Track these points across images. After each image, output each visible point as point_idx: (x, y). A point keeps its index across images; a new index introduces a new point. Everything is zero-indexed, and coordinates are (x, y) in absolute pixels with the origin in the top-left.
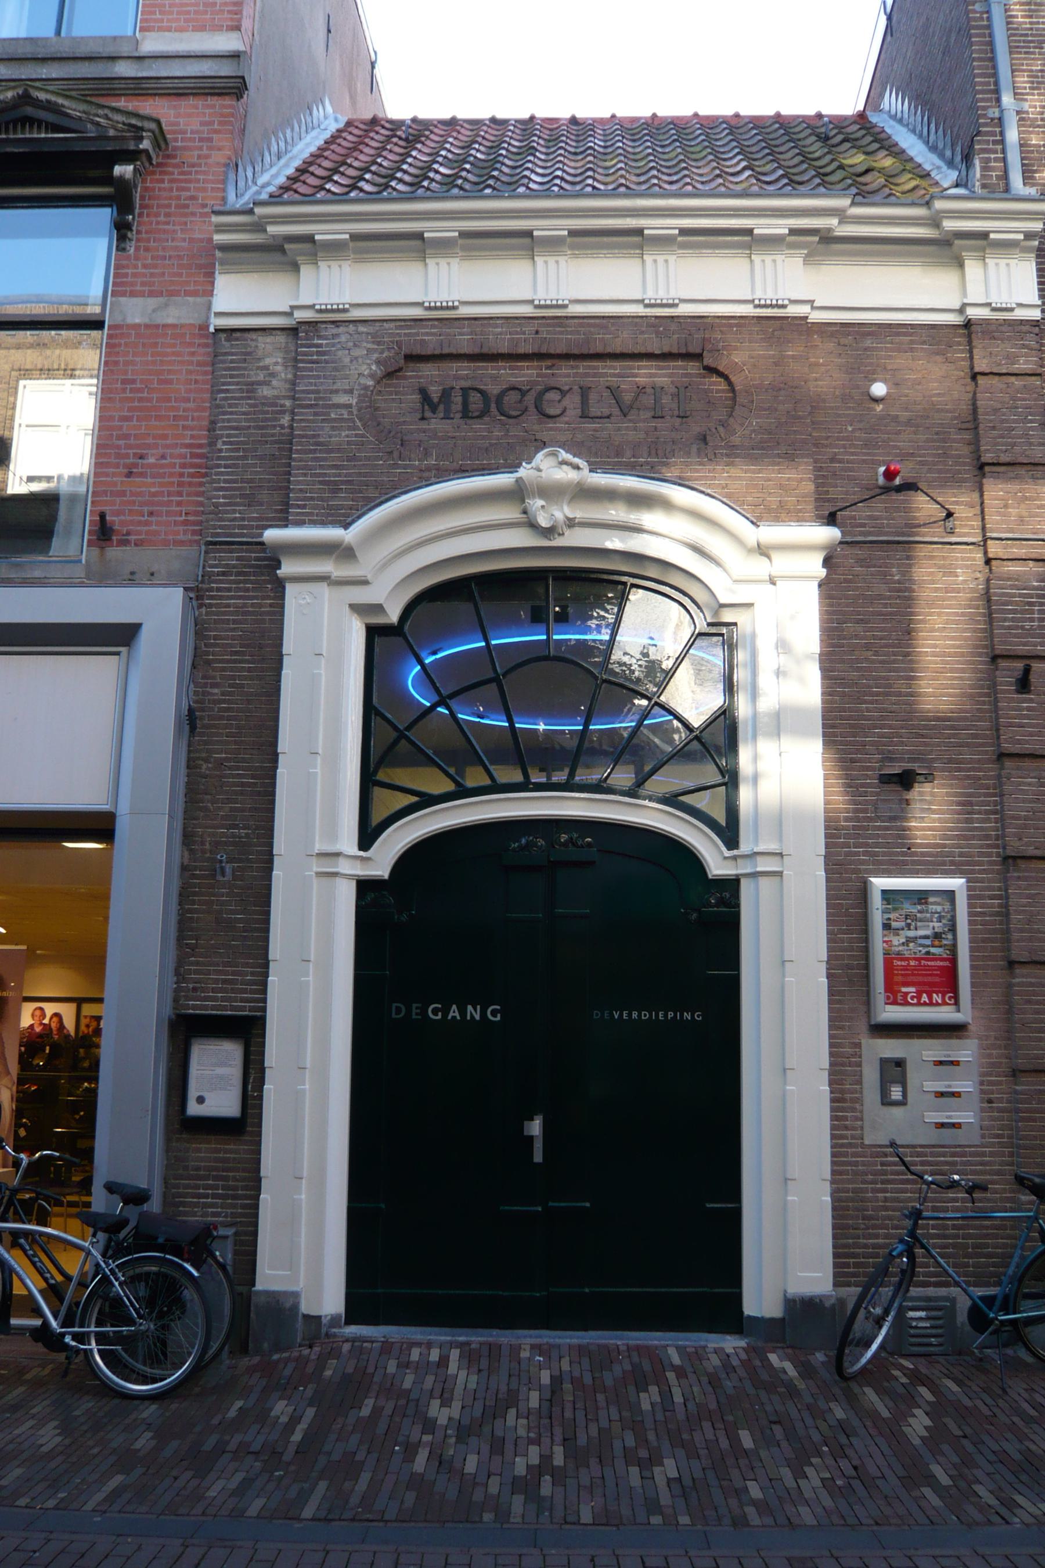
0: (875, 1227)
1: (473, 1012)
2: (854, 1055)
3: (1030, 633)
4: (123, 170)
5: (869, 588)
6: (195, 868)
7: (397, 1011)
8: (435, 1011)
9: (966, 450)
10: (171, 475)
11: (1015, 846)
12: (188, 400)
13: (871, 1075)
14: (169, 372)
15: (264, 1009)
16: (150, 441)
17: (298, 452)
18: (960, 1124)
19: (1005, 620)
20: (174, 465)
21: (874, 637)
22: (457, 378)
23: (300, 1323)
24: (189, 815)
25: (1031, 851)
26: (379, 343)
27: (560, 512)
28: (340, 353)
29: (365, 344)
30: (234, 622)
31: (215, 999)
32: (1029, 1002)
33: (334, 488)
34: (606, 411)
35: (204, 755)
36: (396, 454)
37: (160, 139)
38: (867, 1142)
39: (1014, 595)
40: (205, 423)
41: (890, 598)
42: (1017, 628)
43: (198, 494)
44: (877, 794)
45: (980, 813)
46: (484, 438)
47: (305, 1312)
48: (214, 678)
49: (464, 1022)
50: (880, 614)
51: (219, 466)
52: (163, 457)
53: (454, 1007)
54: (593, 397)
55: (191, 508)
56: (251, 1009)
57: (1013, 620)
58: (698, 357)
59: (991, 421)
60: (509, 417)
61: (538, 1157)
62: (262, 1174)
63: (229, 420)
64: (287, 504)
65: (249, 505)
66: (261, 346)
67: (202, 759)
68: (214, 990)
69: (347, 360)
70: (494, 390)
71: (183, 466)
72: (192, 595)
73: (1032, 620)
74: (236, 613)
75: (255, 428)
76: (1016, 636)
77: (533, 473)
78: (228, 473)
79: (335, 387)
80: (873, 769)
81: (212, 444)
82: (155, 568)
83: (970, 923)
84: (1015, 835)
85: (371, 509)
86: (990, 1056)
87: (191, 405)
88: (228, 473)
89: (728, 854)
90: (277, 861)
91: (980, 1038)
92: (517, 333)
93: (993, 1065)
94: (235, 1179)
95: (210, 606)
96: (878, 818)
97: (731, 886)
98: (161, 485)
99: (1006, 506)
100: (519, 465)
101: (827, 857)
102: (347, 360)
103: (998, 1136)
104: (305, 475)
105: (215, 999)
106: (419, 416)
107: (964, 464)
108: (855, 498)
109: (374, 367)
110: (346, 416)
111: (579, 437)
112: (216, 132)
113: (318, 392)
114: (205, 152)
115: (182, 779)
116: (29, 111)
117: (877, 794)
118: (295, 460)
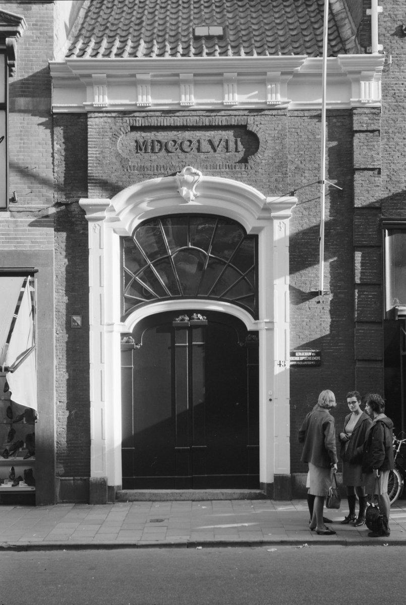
97: (256, 333)
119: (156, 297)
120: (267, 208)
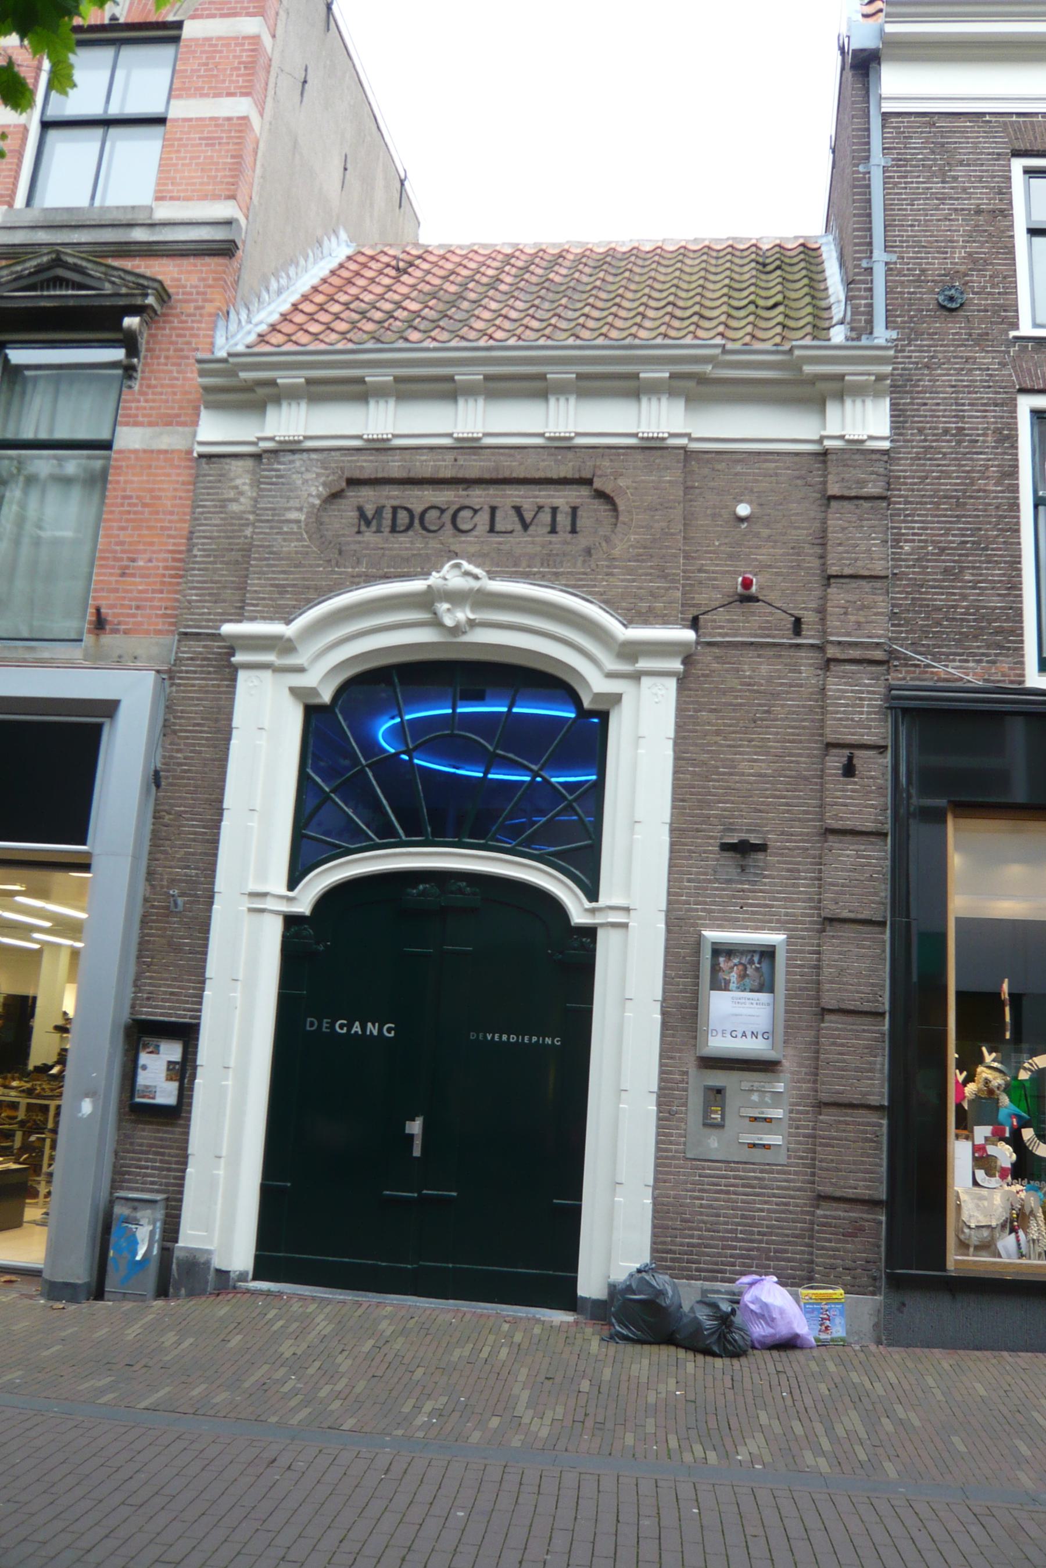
0: (691, 1229)
1: (372, 1029)
2: (682, 1082)
3: (860, 724)
4: (131, 322)
5: (723, 682)
6: (155, 900)
7: (311, 1024)
8: (341, 1027)
9: (816, 563)
10: (156, 575)
11: (831, 909)
12: (172, 513)
13: (695, 1100)
14: (160, 489)
15: (199, 1018)
16: (141, 547)
17: (255, 559)
18: (769, 1145)
19: (837, 712)
20: (158, 568)
21: (725, 725)
22: (388, 498)
23: (211, 1276)
24: (152, 858)
25: (845, 914)
26: (326, 469)
27: (462, 615)
28: (294, 476)
29: (314, 469)
30: (198, 699)
31: (164, 1007)
32: (834, 1044)
33: (282, 590)
34: (509, 528)
35: (166, 807)
36: (333, 562)
37: (164, 296)
38: (688, 1156)
39: (846, 691)
40: (185, 533)
41: (740, 691)
42: (847, 719)
43: (176, 592)
44: (718, 860)
45: (805, 879)
46: (407, 549)
47: (218, 1267)
48: (178, 744)
49: (364, 1038)
50: (731, 704)
51: (194, 569)
52: (150, 560)
53: (357, 1024)
54: (499, 514)
55: (169, 604)
56: (191, 1017)
57: (844, 712)
58: (589, 482)
59: (839, 538)
60: (429, 531)
61: (417, 1152)
62: (190, 1151)
63: (204, 531)
64: (243, 601)
65: (216, 602)
66: (233, 468)
67: (165, 811)
68: (163, 1000)
69: (299, 482)
70: (418, 509)
71: (166, 568)
72: (164, 676)
73: (862, 713)
74: (199, 692)
75: (224, 537)
76: (845, 727)
77: (441, 582)
78: (200, 576)
79: (289, 505)
80: (715, 838)
81: (190, 551)
82: (139, 652)
83: (788, 973)
84: (832, 899)
85: (310, 608)
86: (799, 1089)
87: (175, 517)
88: (200, 576)
89: (588, 905)
90: (217, 897)
91: (792, 1073)
92: (438, 460)
93: (802, 1097)
94: (170, 1155)
95: (179, 685)
96: (717, 880)
97: (590, 932)
98: (148, 584)
99: (845, 613)
100: (430, 574)
101: (669, 912)
102: (299, 482)
103: (802, 1158)
104: (259, 579)
105: (164, 1007)
106: (356, 530)
107: (814, 575)
108: (717, 604)
109: (321, 489)
110: (295, 530)
111: (486, 549)
112: (210, 287)
113: (274, 509)
114: (200, 304)
115: (149, 827)
116: (61, 272)
117: (718, 860)
118: (252, 566)
119: (372, 839)
120: (630, 651)
